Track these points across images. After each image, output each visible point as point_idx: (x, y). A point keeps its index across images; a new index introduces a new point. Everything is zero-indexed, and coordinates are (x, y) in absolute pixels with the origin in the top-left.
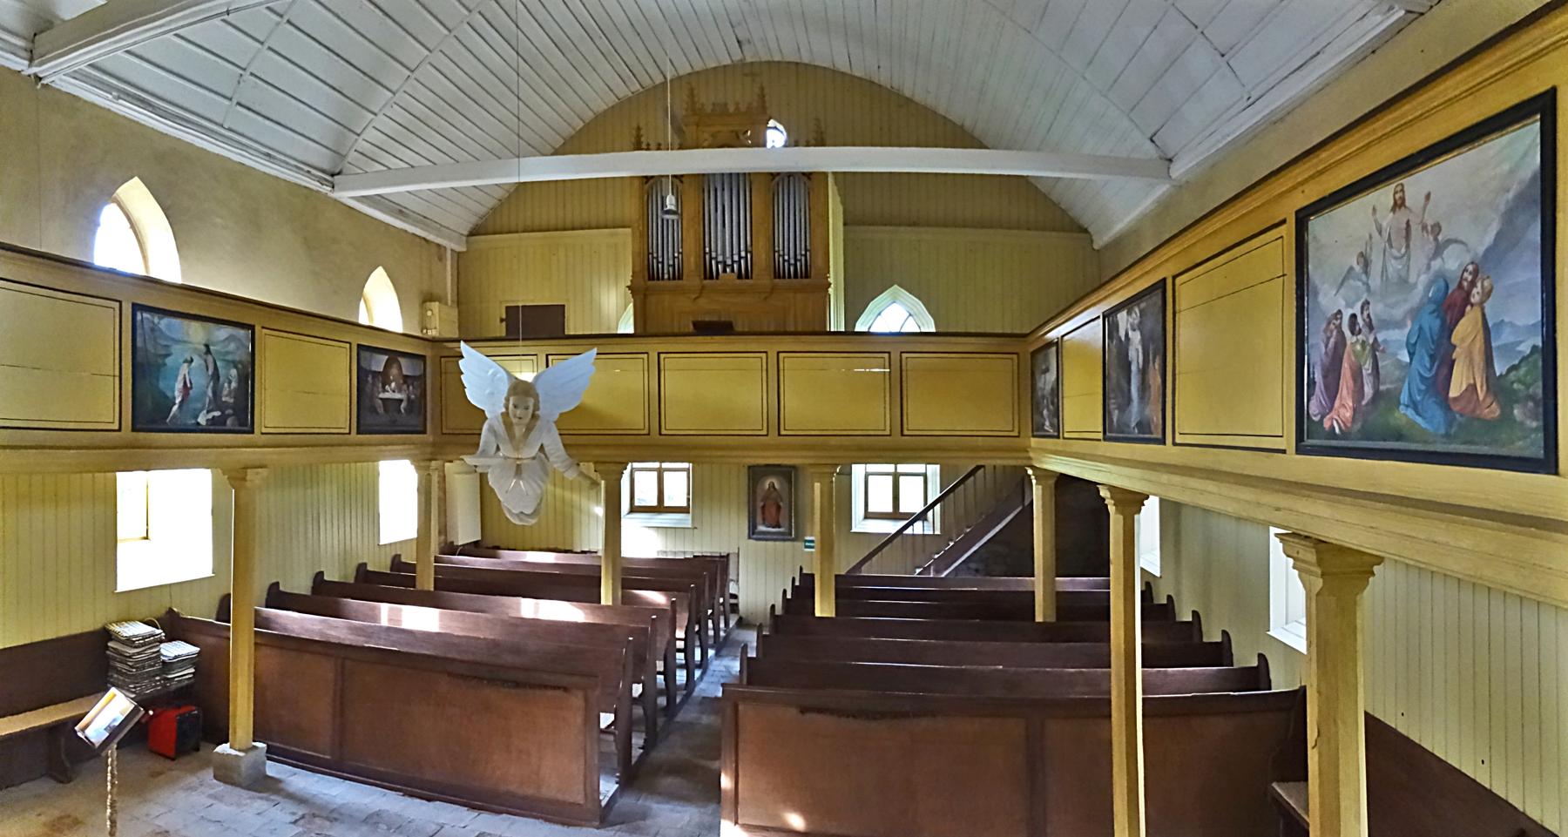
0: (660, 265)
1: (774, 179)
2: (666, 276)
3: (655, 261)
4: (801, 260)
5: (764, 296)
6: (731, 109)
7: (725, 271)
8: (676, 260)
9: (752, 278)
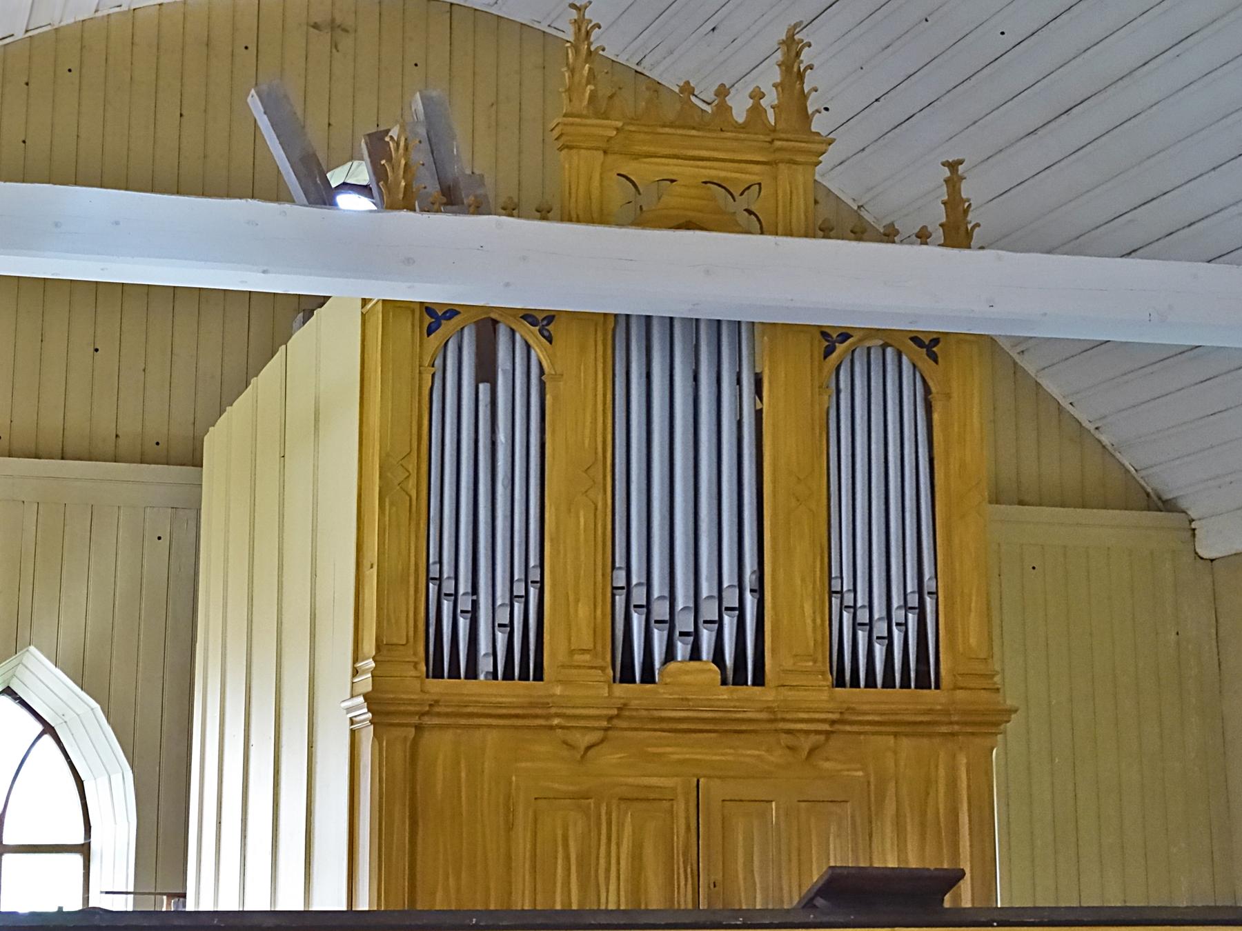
0: (463, 623)
1: (828, 352)
2: (485, 665)
3: (847, 616)
4: (903, 625)
5: (806, 743)
6: (739, 107)
7: (670, 655)
8: (518, 607)
9: (937, 687)
